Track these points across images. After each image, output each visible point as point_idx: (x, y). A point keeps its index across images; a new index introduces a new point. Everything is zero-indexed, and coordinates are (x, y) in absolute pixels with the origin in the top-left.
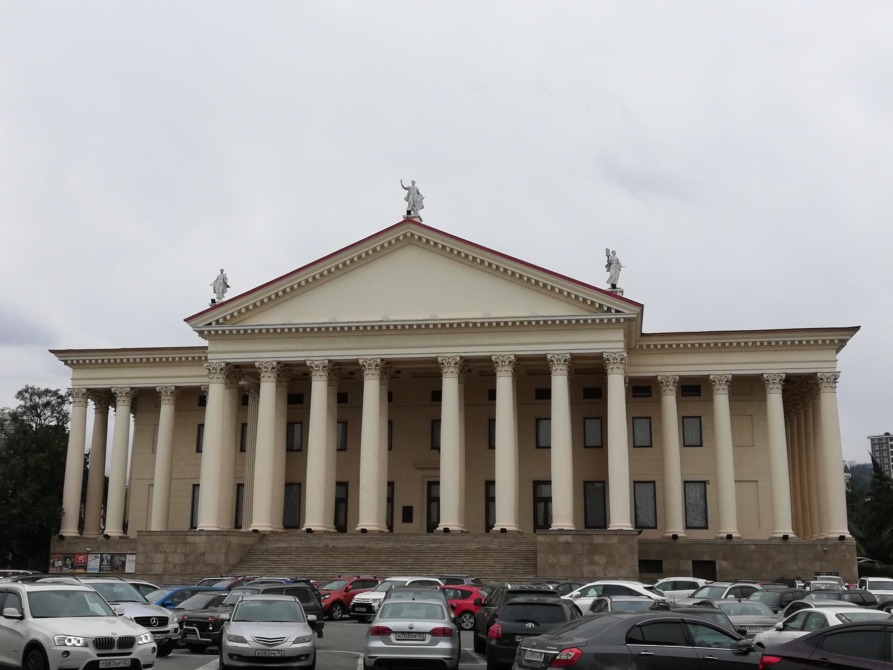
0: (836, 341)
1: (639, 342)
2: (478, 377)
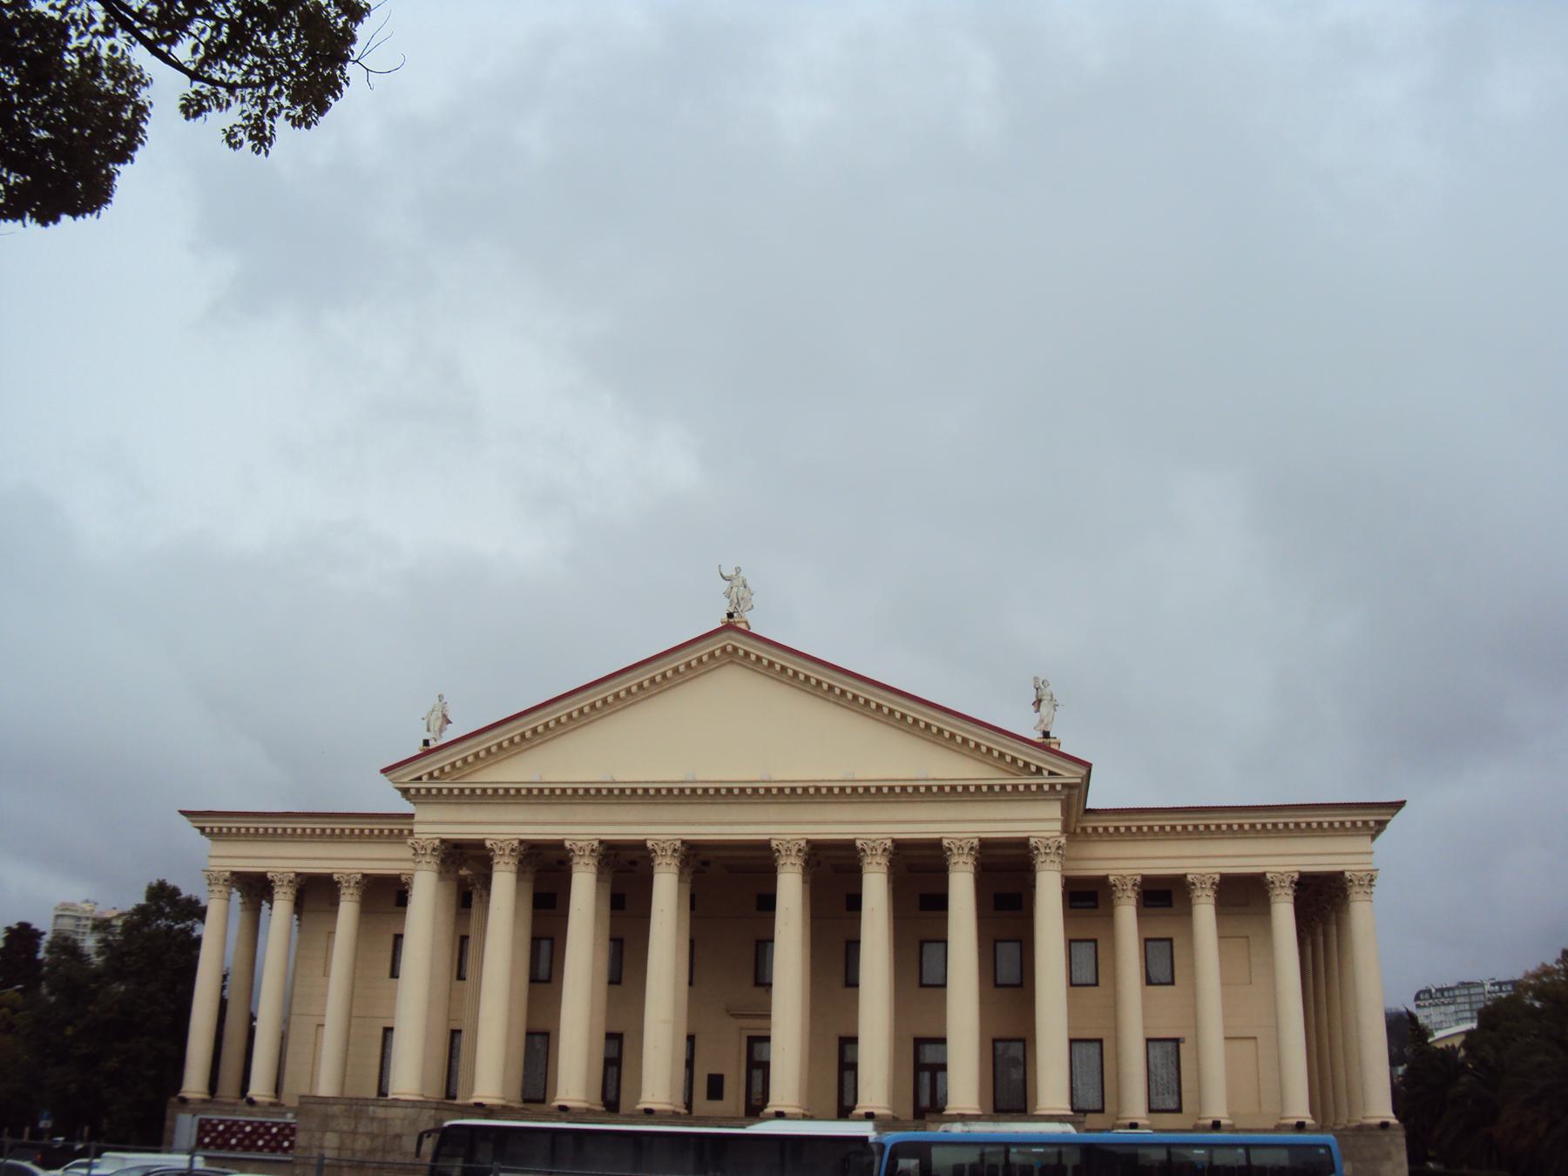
0: (1372, 824)
1: (1081, 820)
2: (834, 870)
